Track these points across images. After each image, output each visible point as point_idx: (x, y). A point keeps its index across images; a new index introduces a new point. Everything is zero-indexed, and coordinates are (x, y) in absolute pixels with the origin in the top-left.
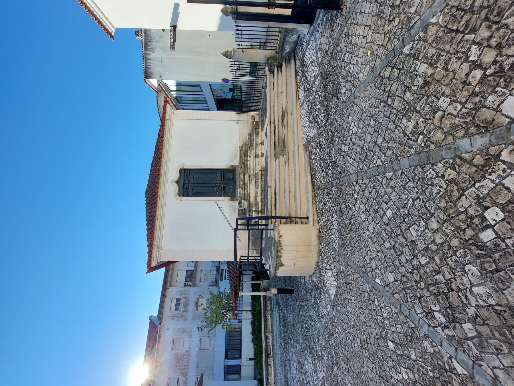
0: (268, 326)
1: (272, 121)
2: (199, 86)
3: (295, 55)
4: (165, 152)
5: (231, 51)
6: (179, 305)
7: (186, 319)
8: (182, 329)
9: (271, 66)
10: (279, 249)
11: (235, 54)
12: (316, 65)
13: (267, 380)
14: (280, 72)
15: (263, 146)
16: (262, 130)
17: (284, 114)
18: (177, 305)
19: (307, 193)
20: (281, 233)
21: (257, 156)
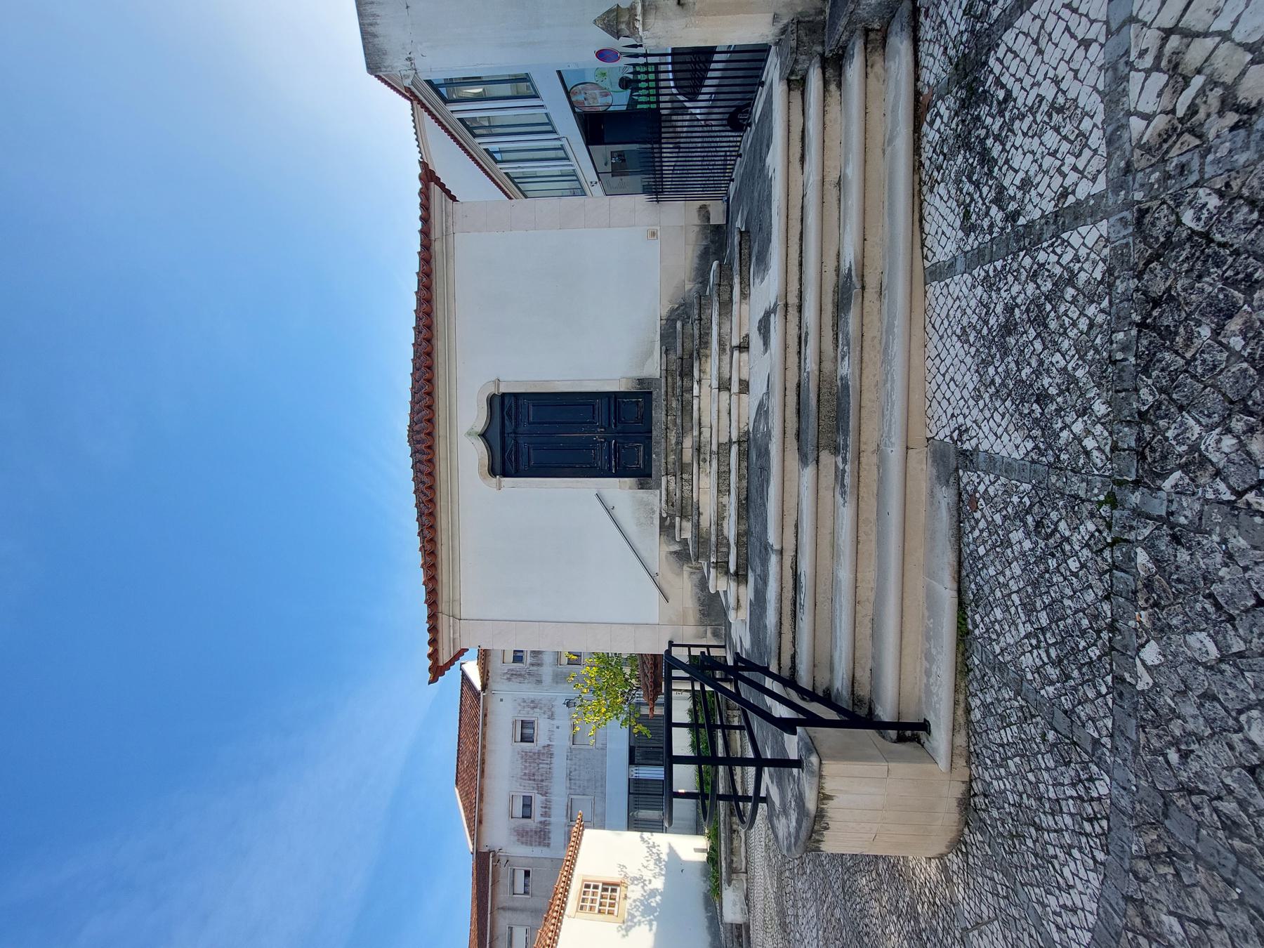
0: (732, 744)
1: (793, 300)
2: (525, 79)
4: (440, 345)
7: (539, 682)
8: (533, 702)
12: (1096, 139)
14: (833, 87)
15: (744, 355)
17: (845, 293)
20: (829, 787)
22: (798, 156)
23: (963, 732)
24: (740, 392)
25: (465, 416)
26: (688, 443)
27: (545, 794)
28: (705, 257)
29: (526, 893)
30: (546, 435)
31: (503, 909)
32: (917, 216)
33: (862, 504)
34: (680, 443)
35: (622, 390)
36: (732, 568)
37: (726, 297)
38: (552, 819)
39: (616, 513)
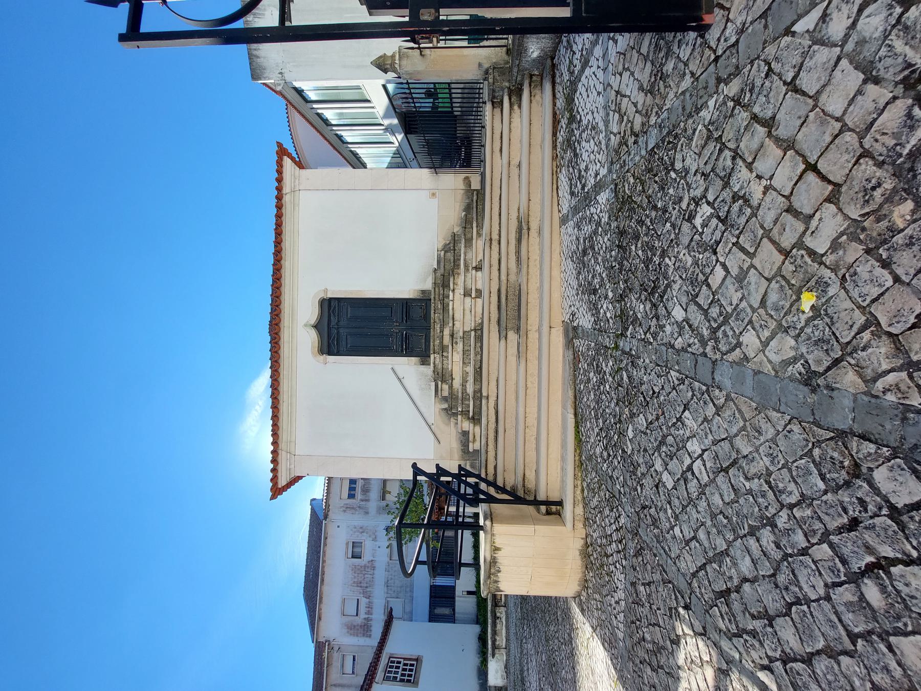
1: (495, 237)
3: (554, 66)
5: (393, 56)
6: (354, 489)
7: (367, 513)
9: (494, 91)
10: (493, 571)
11: (404, 62)
13: (494, 641)
14: (516, 107)
15: (479, 273)
16: (479, 235)
18: (352, 489)
19: (563, 459)
20: (498, 542)
21: (467, 294)
22: (499, 148)
23: (581, 506)
24: (476, 297)
25: (302, 313)
26: (447, 332)
27: (369, 597)
28: (468, 209)
29: (353, 673)
30: (360, 327)
31: (335, 685)
32: (555, 186)
33: (529, 364)
34: (442, 331)
35: (411, 297)
36: (471, 414)
37: (469, 236)
38: (373, 617)
39: (405, 381)
